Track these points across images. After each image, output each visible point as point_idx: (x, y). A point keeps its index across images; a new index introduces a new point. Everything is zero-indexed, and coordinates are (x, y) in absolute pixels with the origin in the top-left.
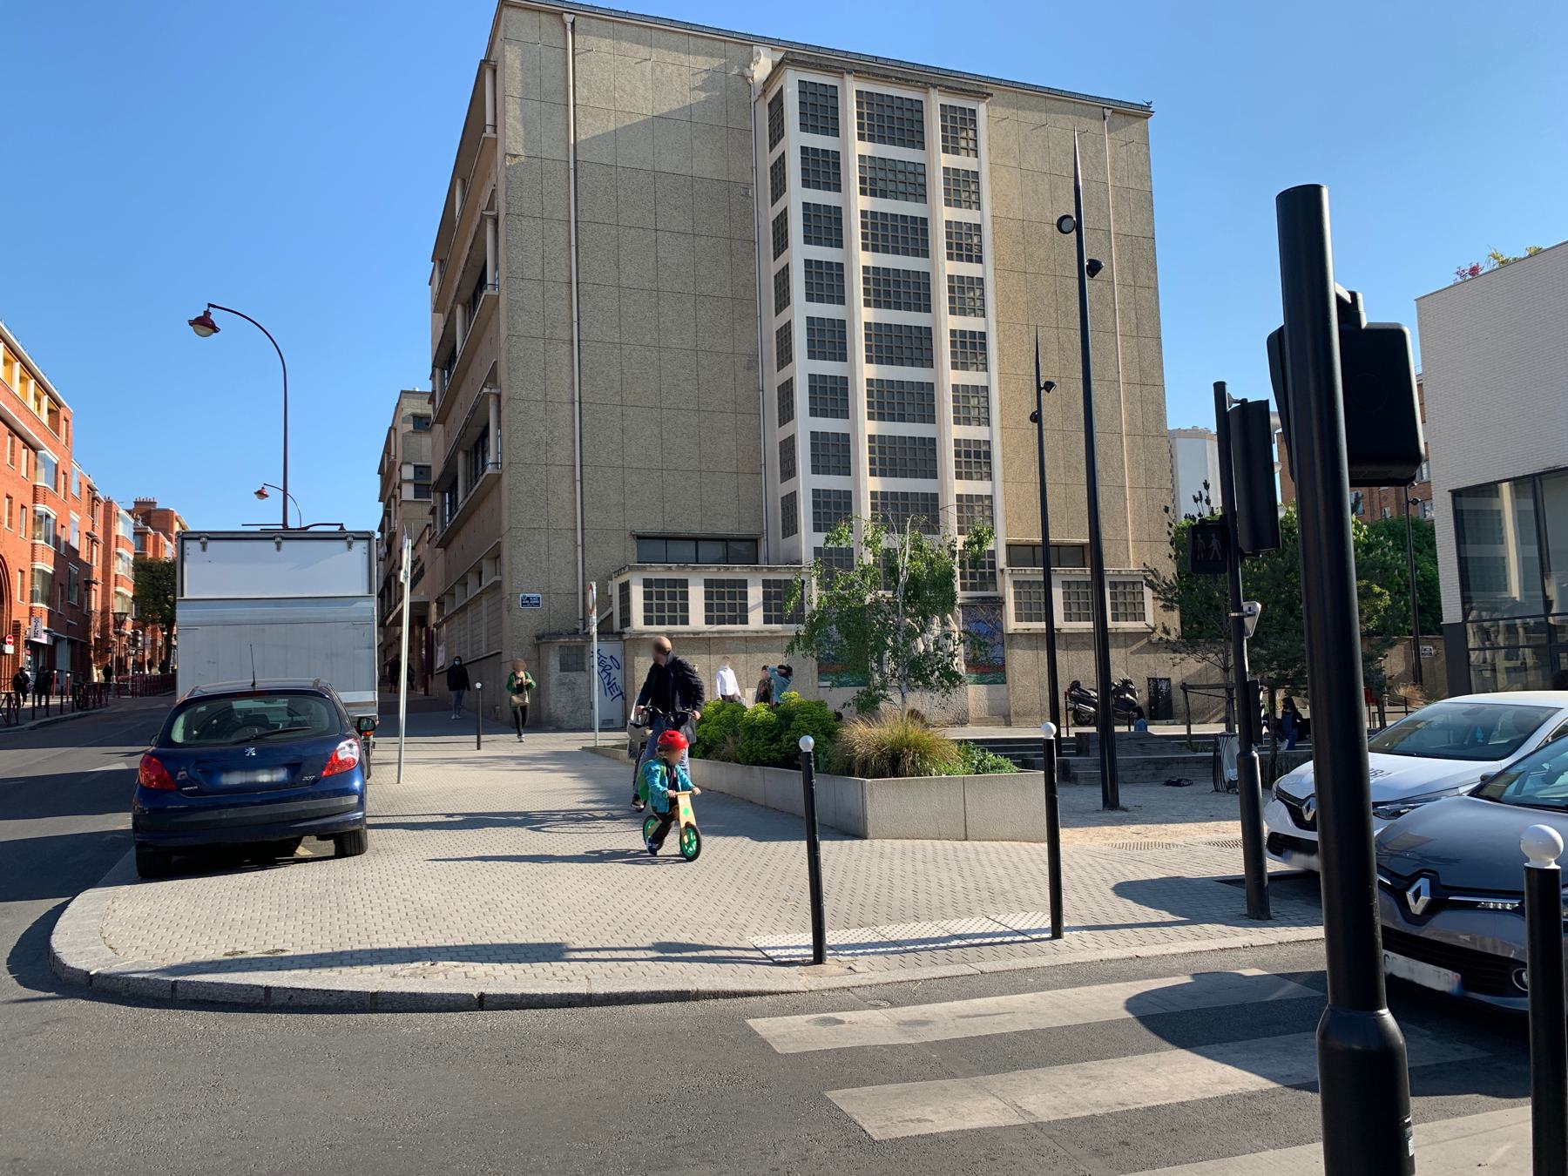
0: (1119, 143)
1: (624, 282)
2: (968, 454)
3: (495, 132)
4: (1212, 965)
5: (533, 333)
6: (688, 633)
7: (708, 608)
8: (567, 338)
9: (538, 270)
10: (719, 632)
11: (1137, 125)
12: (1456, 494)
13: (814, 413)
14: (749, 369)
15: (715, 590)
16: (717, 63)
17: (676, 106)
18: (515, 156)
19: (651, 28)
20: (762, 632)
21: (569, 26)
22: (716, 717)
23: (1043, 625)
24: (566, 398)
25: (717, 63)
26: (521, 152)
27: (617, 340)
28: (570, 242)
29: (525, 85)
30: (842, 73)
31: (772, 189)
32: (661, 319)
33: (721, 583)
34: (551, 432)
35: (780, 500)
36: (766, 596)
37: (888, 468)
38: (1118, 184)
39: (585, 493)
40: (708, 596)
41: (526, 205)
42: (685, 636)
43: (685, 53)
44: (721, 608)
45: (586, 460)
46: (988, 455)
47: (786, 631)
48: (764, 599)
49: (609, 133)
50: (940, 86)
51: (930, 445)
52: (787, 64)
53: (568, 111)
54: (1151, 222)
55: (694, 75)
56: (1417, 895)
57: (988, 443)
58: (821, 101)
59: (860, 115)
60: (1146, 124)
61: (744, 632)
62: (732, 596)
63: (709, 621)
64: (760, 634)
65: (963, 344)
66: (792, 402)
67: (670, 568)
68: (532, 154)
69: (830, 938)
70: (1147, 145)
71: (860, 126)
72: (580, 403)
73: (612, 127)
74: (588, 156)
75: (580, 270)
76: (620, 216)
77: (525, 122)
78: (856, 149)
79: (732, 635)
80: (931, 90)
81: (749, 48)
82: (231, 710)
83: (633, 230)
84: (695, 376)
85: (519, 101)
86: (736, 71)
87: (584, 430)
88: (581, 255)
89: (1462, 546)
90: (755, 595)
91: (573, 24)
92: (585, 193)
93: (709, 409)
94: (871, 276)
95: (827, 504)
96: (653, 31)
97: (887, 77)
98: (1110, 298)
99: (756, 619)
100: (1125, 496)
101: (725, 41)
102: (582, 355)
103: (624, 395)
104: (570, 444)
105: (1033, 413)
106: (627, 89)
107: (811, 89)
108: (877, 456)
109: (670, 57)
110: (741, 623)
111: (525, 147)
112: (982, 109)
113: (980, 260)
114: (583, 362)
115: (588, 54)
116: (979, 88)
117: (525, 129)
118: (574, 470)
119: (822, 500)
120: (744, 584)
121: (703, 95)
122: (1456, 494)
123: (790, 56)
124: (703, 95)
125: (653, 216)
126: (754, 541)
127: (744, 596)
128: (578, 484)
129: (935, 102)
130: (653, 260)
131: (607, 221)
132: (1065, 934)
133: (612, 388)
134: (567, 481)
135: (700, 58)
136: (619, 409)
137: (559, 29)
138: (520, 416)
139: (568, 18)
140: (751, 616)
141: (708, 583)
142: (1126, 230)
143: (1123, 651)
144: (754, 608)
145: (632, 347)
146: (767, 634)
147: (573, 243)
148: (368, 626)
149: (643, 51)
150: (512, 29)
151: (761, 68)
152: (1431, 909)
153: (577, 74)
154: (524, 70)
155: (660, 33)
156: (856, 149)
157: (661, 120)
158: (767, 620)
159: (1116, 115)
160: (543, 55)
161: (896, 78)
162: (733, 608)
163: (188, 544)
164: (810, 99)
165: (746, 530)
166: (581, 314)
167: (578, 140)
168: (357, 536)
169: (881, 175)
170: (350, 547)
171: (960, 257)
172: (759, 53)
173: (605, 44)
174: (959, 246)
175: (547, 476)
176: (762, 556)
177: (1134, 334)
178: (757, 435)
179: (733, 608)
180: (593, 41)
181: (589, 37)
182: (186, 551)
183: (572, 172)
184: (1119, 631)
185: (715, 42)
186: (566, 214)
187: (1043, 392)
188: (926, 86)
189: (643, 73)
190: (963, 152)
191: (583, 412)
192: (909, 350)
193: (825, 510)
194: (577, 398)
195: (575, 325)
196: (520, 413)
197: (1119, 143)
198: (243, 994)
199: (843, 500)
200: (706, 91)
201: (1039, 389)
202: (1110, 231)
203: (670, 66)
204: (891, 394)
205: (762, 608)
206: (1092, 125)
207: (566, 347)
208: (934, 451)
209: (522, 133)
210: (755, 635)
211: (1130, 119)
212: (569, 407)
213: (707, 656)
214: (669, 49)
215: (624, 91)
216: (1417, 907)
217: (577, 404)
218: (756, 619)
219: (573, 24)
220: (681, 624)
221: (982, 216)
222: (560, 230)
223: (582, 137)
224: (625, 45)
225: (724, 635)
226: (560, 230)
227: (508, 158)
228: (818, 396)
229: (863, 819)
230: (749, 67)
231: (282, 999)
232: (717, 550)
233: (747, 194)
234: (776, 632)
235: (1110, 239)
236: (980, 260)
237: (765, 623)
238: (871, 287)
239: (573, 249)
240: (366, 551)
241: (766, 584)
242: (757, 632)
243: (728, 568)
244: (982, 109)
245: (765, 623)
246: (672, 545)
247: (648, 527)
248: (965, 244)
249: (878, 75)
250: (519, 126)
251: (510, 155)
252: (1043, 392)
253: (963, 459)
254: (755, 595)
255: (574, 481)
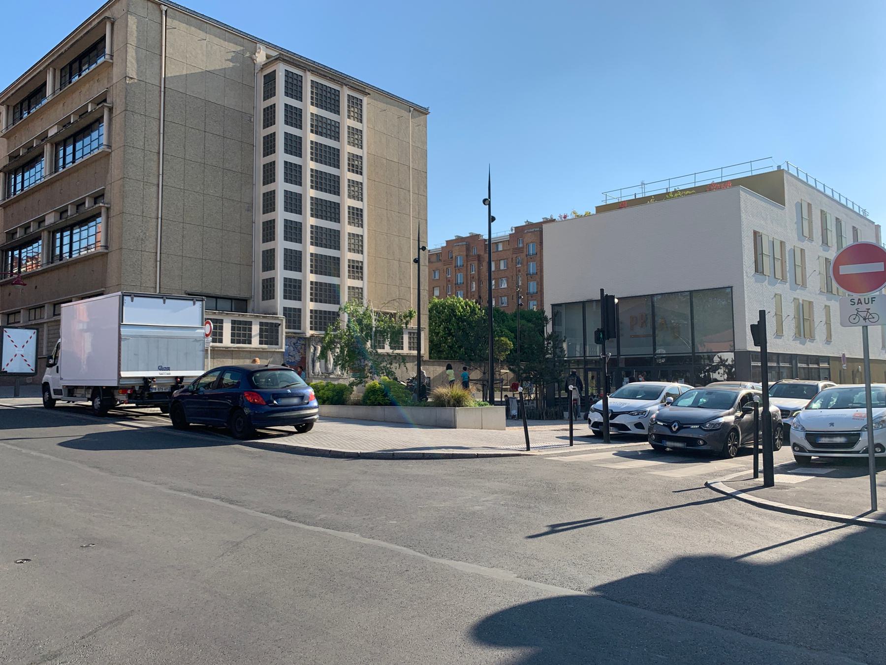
0: (415, 125)
1: (187, 157)
2: (353, 267)
3: (112, 59)
4: (620, 450)
5: (138, 178)
6: (223, 347)
7: (233, 335)
8: (156, 182)
9: (142, 144)
10: (238, 348)
11: (423, 117)
12: (553, 306)
13: (286, 239)
14: (248, 211)
15: (236, 326)
16: (239, 48)
17: (217, 68)
18: (132, 78)
19: (207, 23)
20: (259, 348)
21: (164, 12)
22: (327, 387)
23: (588, 355)
24: (154, 215)
25: (239, 48)
26: (135, 77)
27: (182, 188)
28: (160, 130)
29: (139, 40)
30: (305, 70)
31: (264, 120)
32: (206, 179)
33: (240, 322)
34: (145, 233)
35: (261, 282)
36: (261, 330)
37: (318, 270)
38: (414, 144)
39: (162, 269)
40: (233, 329)
41: (136, 107)
42: (221, 349)
43: (223, 40)
44: (239, 335)
45: (164, 251)
46: (362, 268)
47: (269, 348)
48: (260, 332)
49: (182, 75)
50: (348, 85)
51: (337, 261)
52: (280, 60)
53: (161, 59)
54: (426, 165)
55: (227, 52)
56: (675, 426)
57: (362, 262)
58: (295, 82)
59: (312, 93)
60: (426, 117)
61: (250, 348)
62: (245, 329)
63: (233, 342)
64: (257, 350)
65: (353, 213)
66: (274, 231)
67: (215, 313)
68: (141, 79)
69: (531, 445)
70: (426, 127)
71: (312, 98)
72: (161, 219)
73: (184, 73)
74: (171, 86)
75: (165, 147)
76: (187, 121)
77: (138, 61)
78: (310, 110)
79: (244, 349)
80: (344, 87)
81: (254, 44)
82: (275, 375)
83: (193, 130)
84: (221, 212)
85: (134, 48)
86: (248, 55)
87: (162, 234)
88: (165, 139)
89: (554, 326)
90: (256, 329)
91: (166, 11)
92: (169, 106)
93: (228, 229)
94: (314, 174)
95: (290, 286)
96: (208, 25)
97: (326, 76)
98: (408, 198)
99: (255, 342)
100: (410, 292)
101: (243, 38)
102: (164, 193)
103: (184, 217)
104: (155, 240)
105: (416, 259)
106: (193, 53)
107: (290, 75)
108: (313, 264)
109: (216, 40)
110: (248, 344)
111: (137, 74)
112: (365, 100)
113: (361, 174)
114: (164, 197)
115: (174, 30)
116: (362, 88)
117: (138, 64)
118: (156, 255)
119: (288, 283)
120: (250, 323)
121: (231, 65)
122: (553, 306)
123: (282, 56)
124: (231, 65)
125: (203, 124)
126: (245, 301)
127: (250, 329)
128: (158, 263)
129: (345, 93)
130: (203, 147)
131: (180, 123)
132: (574, 445)
133: (178, 213)
134: (152, 261)
135: (231, 44)
136: (181, 224)
137: (158, 12)
138: (129, 223)
139: (164, 8)
140: (253, 340)
141: (233, 322)
142: (415, 167)
143: (411, 364)
144: (255, 336)
145: (190, 192)
146: (261, 350)
147: (162, 131)
148: (202, 341)
149: (202, 34)
150: (132, 6)
151: (261, 57)
152: (678, 430)
153: (167, 40)
154: (138, 31)
155: (211, 27)
156: (310, 110)
157: (210, 74)
158: (261, 343)
159: (415, 111)
160: (148, 25)
161: (330, 78)
162: (245, 335)
163: (125, 298)
164: (290, 80)
165: (243, 295)
166: (164, 171)
167: (166, 76)
168: (136, 295)
169: (320, 124)
170: (194, 304)
171: (353, 171)
172: (260, 48)
173: (183, 26)
174: (353, 166)
175: (141, 257)
176: (249, 309)
177: (417, 217)
178: (250, 245)
179: (245, 335)
180: (176, 23)
181: (175, 21)
182: (124, 301)
183: (162, 93)
184: (411, 355)
185: (239, 37)
186: (158, 115)
187: (421, 250)
188: (342, 84)
189: (202, 46)
190: (352, 118)
191: (163, 224)
192: (334, 214)
193: (289, 289)
194: (160, 216)
195: (161, 176)
196: (129, 221)
197: (415, 125)
198: (416, 455)
199: (297, 284)
200: (233, 63)
201: (419, 249)
202: (410, 166)
203: (216, 45)
204: (321, 234)
205: (258, 336)
206: (405, 114)
207: (154, 189)
208: (339, 264)
209: (136, 66)
210: (255, 350)
211: (421, 114)
212: (155, 220)
213: (231, 360)
214: (216, 36)
215: (191, 54)
216: (674, 429)
217: (160, 220)
218: (255, 342)
219: (166, 11)
220: (219, 342)
221: (363, 152)
222: (155, 124)
223: (168, 75)
224: (193, 28)
225: (240, 349)
226: (155, 124)
227: (128, 79)
228: (288, 230)
229: (455, 421)
230: (255, 54)
231: (428, 456)
232: (227, 304)
233: (251, 120)
234: (265, 349)
235: (410, 170)
236: (361, 174)
237: (260, 344)
238: (314, 179)
239: (162, 135)
240: (201, 306)
241: (261, 324)
242: (256, 349)
243: (244, 315)
244: (365, 100)
245: (260, 344)
246: (220, 301)
247: (194, 289)
248: (356, 166)
249: (321, 74)
250: (134, 62)
251: (129, 77)
252: (421, 250)
253: (351, 269)
254: (256, 329)
255: (156, 261)
